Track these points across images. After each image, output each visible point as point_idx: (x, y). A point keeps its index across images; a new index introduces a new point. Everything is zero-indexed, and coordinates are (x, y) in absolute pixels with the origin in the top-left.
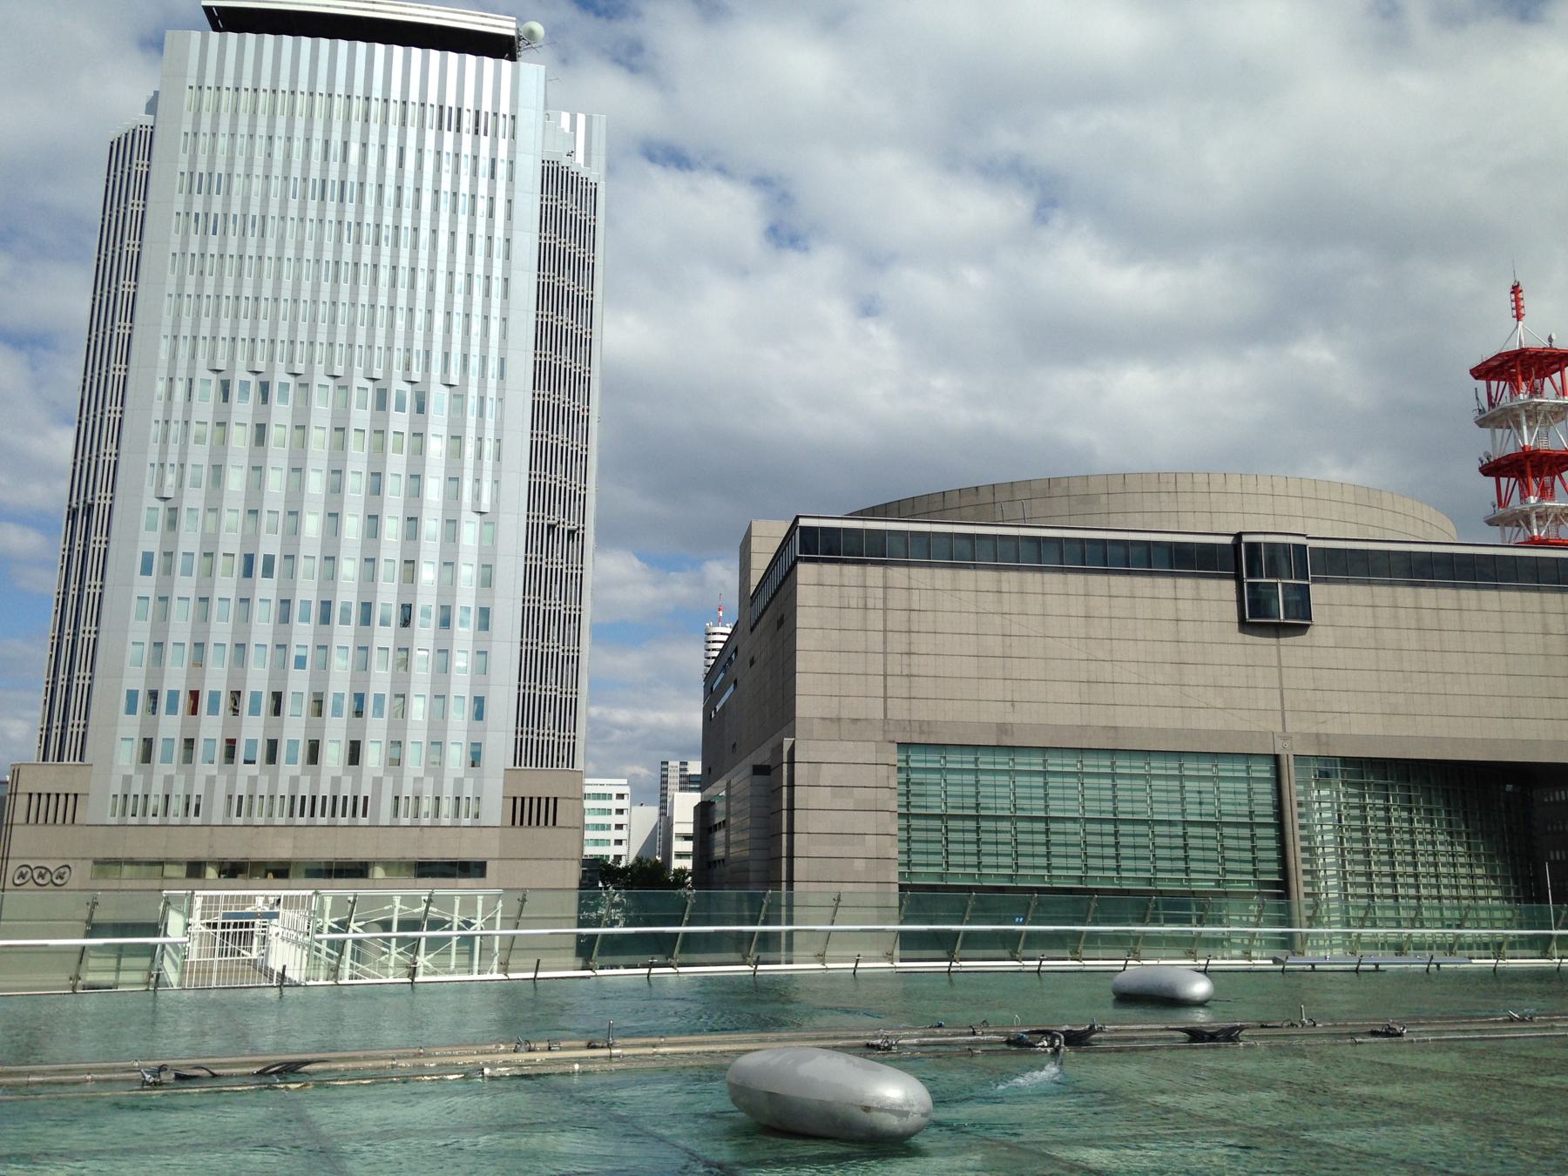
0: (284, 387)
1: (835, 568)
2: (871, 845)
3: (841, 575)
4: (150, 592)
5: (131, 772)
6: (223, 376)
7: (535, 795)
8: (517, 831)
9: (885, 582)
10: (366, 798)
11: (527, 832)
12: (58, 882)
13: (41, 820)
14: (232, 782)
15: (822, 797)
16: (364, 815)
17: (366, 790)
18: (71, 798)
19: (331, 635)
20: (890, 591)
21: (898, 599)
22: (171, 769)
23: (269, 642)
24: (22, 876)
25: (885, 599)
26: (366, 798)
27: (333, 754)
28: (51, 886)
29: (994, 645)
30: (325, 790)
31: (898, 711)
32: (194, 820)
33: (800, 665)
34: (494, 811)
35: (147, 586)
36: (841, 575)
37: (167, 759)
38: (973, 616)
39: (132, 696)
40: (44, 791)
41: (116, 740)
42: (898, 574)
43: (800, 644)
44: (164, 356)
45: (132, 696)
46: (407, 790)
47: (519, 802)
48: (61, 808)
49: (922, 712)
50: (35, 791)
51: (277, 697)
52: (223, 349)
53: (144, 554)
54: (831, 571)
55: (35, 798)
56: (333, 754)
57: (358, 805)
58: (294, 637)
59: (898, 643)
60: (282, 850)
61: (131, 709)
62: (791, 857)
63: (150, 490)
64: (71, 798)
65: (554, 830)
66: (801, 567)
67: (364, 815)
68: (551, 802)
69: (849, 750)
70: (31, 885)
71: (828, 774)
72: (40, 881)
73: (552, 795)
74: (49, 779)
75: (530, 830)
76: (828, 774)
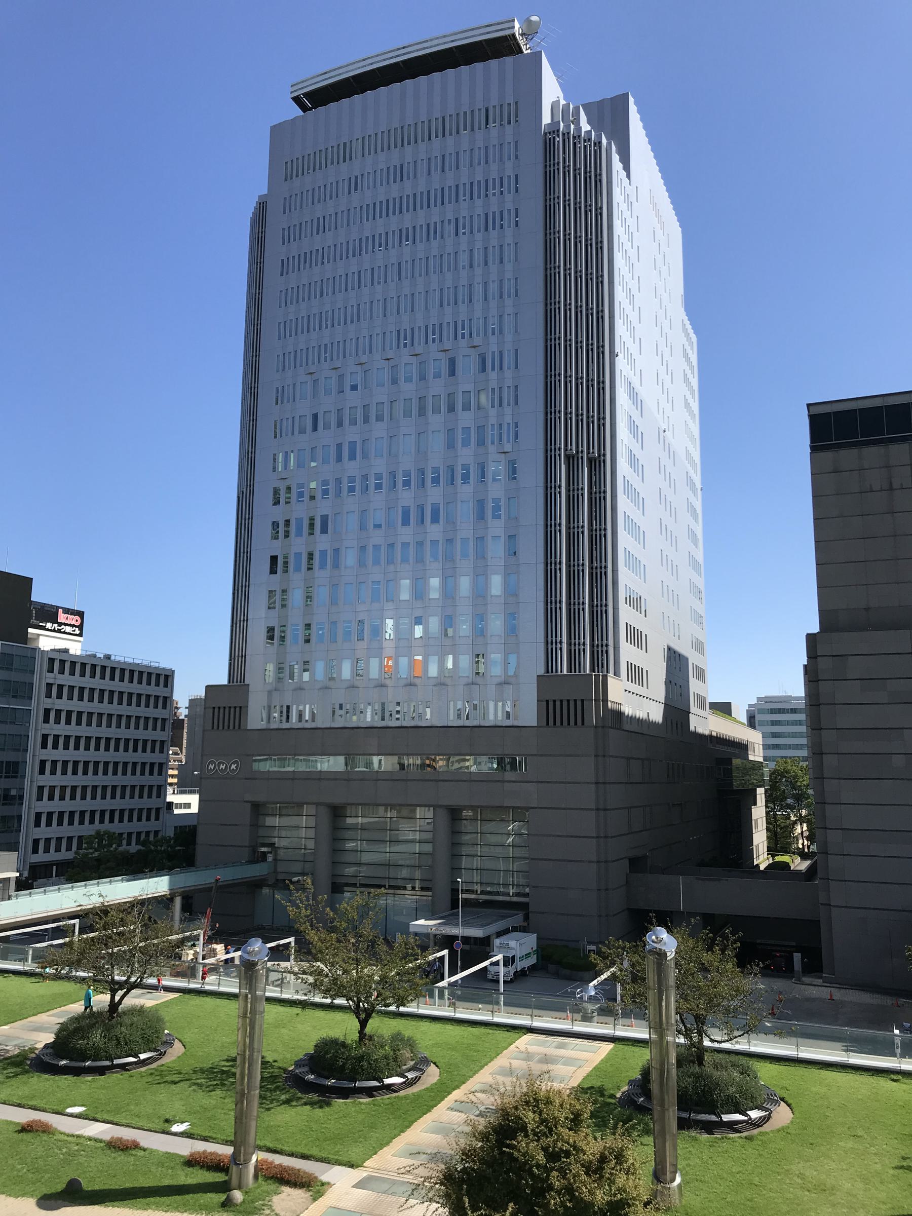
6: (450, 355)
50: (217, 705)
55: (216, 710)
64: (238, 710)
73: (579, 698)
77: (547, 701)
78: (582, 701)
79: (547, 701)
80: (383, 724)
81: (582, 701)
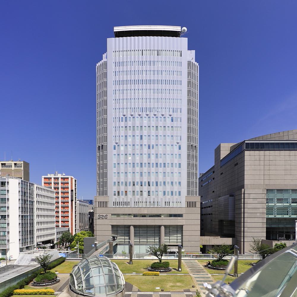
1: (253, 152)
2: (261, 210)
3: (255, 153)
4: (116, 171)
5: (162, 197)
7: (192, 201)
9: (264, 154)
11: (190, 208)
13: (101, 207)
14: (135, 199)
15: (251, 201)
18: (106, 202)
19: (127, 188)
20: (265, 156)
21: (267, 158)
24: (99, 217)
25: (264, 158)
26: (129, 202)
27: (145, 194)
29: (288, 167)
31: (267, 182)
32: (128, 206)
34: (184, 205)
35: (115, 152)
36: (255, 153)
38: (284, 161)
39: (115, 183)
40: (101, 201)
41: (112, 189)
42: (267, 152)
43: (245, 169)
44: (114, 57)
45: (115, 183)
46: (159, 201)
47: (188, 202)
48: (104, 204)
49: (272, 182)
50: (189, 201)
51: (126, 192)
53: (114, 182)
54: (252, 152)
55: (100, 202)
56: (145, 194)
59: (267, 168)
60: (145, 212)
61: (115, 167)
62: (244, 213)
63: (114, 142)
64: (106, 202)
65: (195, 208)
69: (257, 191)
70: (101, 218)
71: (252, 196)
73: (195, 201)
74: (101, 199)
75: (192, 208)
76: (252, 196)
77: (99, 202)
78: (196, 202)
79: (99, 202)
80: (114, 206)
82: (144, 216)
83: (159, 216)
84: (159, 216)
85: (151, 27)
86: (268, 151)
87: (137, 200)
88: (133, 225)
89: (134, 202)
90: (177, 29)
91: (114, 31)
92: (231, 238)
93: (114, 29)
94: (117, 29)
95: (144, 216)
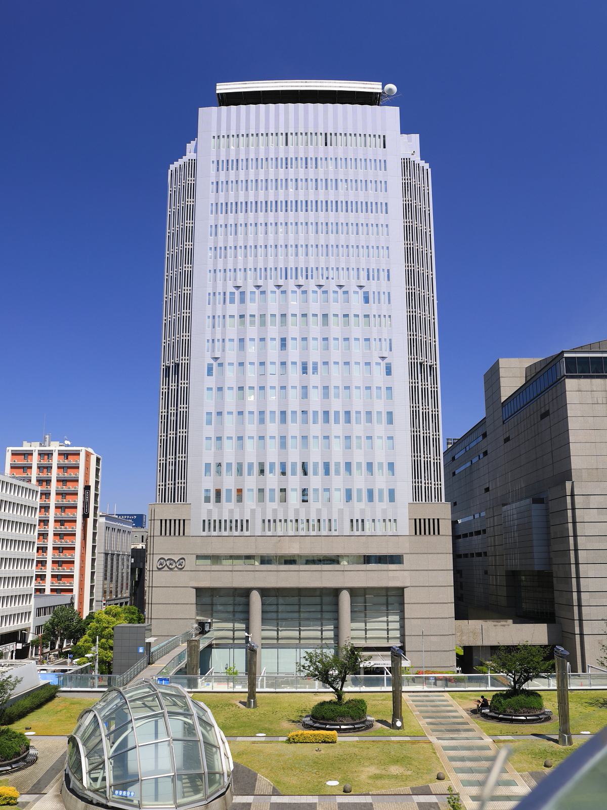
0: (253, 293)
8: (418, 538)
10: (247, 521)
12: (180, 567)
14: (264, 512)
16: (247, 530)
17: (247, 516)
18: (182, 522)
22: (319, 505)
23: (319, 435)
24: (161, 564)
26: (247, 521)
27: (294, 497)
28: (176, 569)
30: (226, 516)
32: (245, 533)
33: (572, 439)
34: (405, 527)
37: (229, 500)
39: (208, 466)
43: (570, 426)
45: (208, 466)
46: (335, 516)
47: (418, 521)
52: (240, 275)
54: (585, 383)
55: (164, 522)
57: (242, 524)
58: (289, 433)
60: (293, 549)
62: (576, 550)
64: (182, 522)
65: (439, 537)
66: (568, 381)
67: (247, 530)
68: (436, 521)
70: (166, 568)
71: (594, 502)
72: (170, 566)
73: (436, 518)
74: (169, 511)
77: (161, 520)
79: (161, 520)
80: (204, 534)
81: (184, 520)
82: (290, 561)
83: (333, 560)
84: (333, 560)
85: (373, 86)
86: (588, 380)
87: (270, 516)
88: (353, 592)
89: (261, 521)
90: (374, 87)
91: (217, 92)
92: (545, 625)
93: (217, 87)
94: (223, 88)
95: (290, 561)
